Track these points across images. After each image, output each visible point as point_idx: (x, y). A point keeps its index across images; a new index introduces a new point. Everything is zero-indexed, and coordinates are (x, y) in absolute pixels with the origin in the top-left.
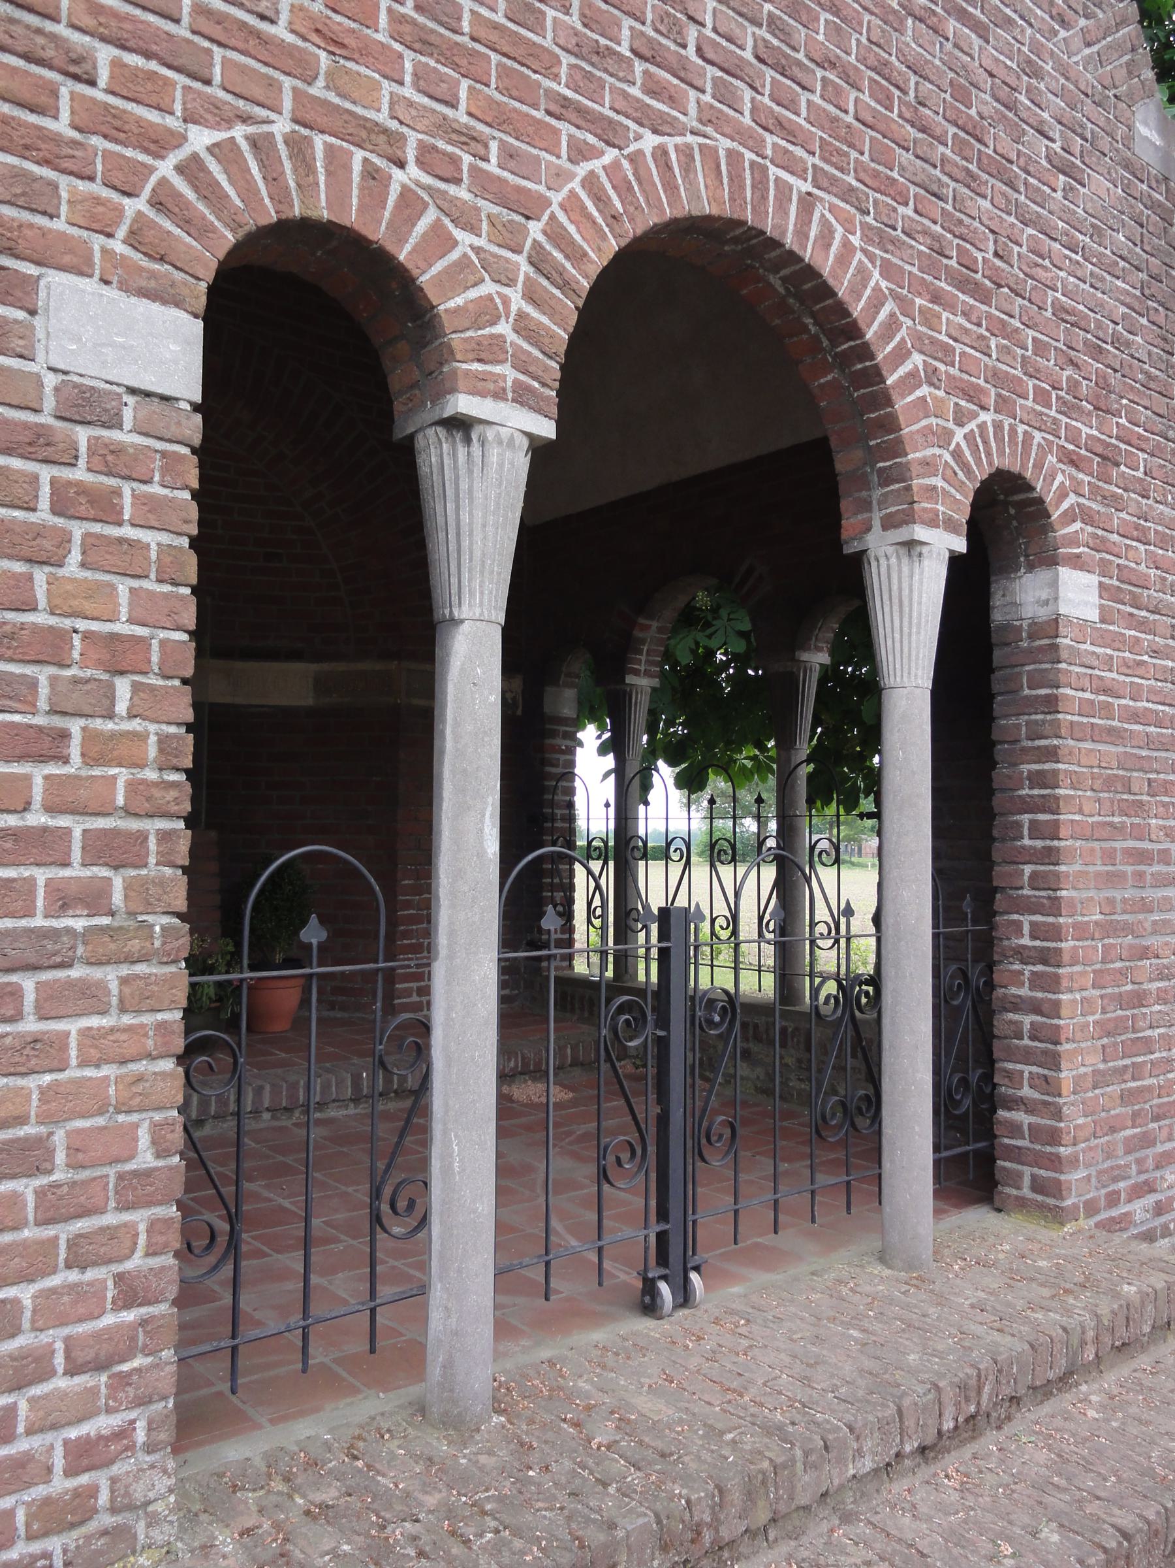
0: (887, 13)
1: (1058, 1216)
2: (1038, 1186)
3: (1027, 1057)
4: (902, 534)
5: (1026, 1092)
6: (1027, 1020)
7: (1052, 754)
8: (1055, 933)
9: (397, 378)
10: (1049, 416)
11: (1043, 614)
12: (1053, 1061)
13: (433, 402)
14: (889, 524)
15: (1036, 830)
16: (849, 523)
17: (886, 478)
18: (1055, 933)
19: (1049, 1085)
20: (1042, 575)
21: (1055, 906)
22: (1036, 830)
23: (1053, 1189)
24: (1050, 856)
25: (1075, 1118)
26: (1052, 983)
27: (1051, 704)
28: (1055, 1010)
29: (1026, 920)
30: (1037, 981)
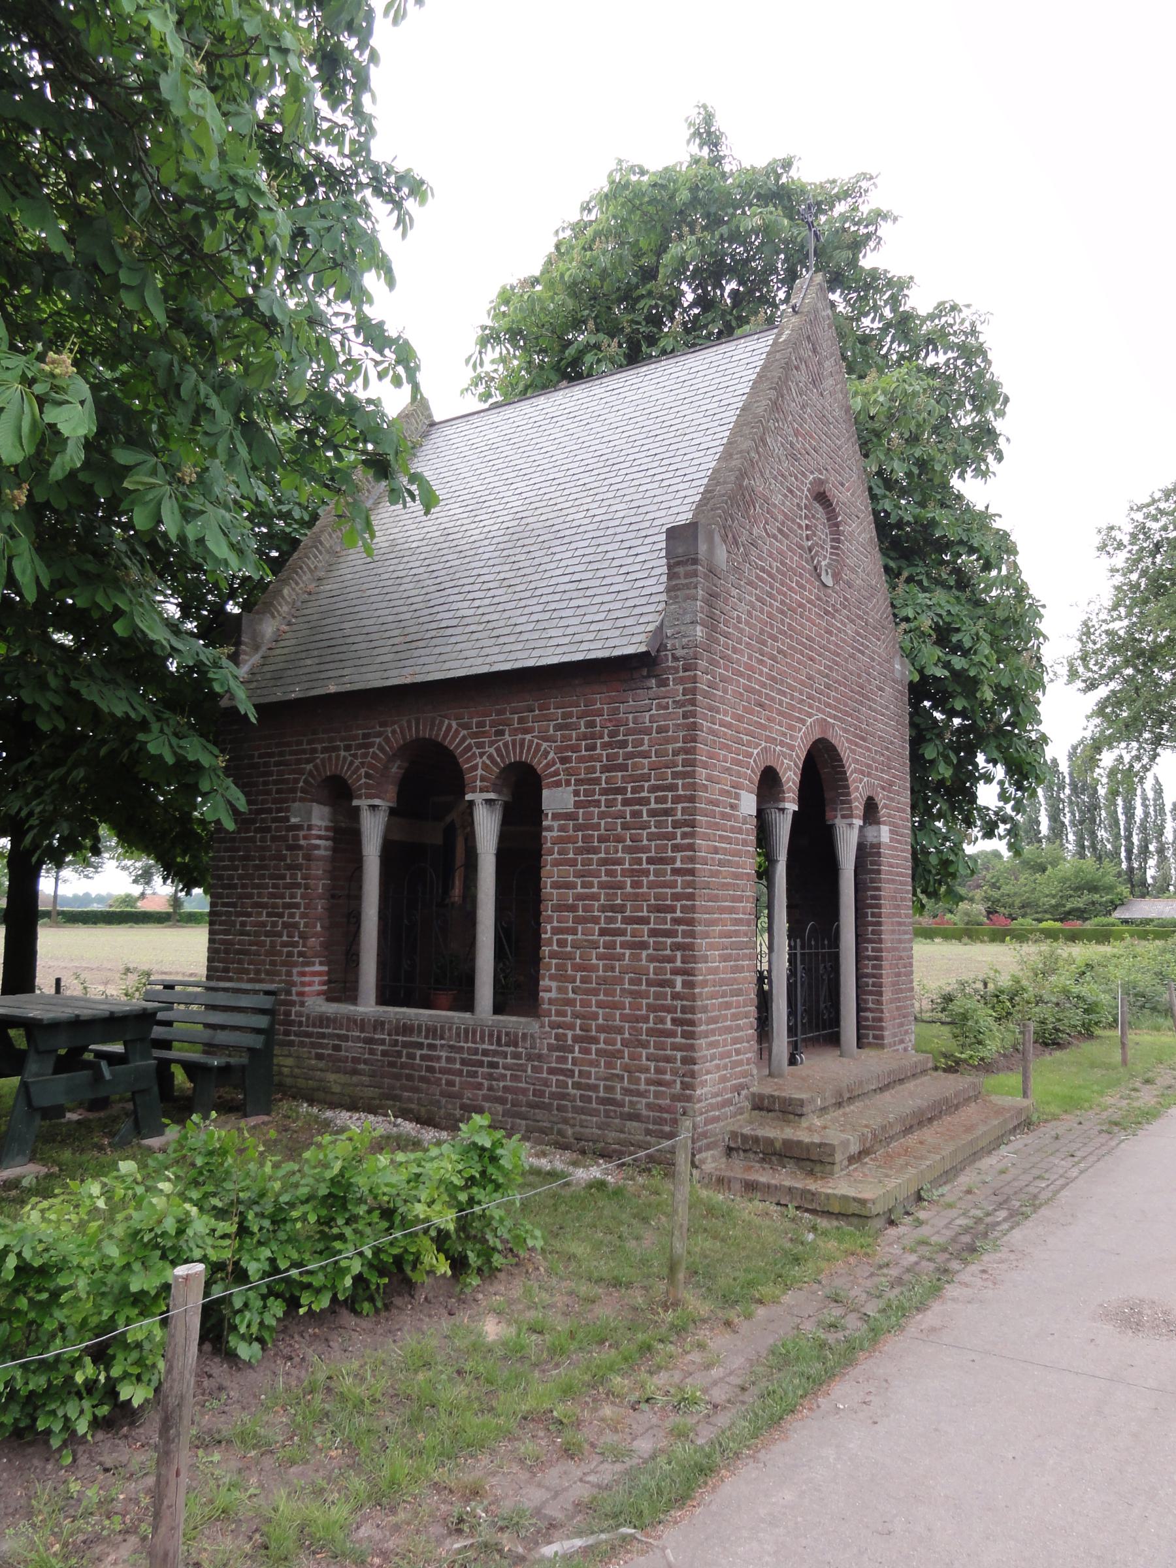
0: (327, 1248)
1: (882, 1046)
2: (875, 1037)
3: (871, 993)
4: (848, 821)
5: (871, 1005)
6: (870, 981)
7: (878, 889)
8: (880, 950)
9: (828, 795)
10: (481, 791)
11: (875, 841)
12: (880, 994)
13: (351, 28)
14: (844, 817)
15: (873, 915)
16: (829, 814)
17: (843, 802)
18: (880, 950)
19: (879, 1002)
20: (874, 827)
21: (880, 941)
22: (873, 915)
23: (882, 1037)
24: (879, 924)
25: (886, 1015)
26: (880, 967)
27: (879, 872)
28: (880, 976)
29: (870, 946)
30: (874, 967)
